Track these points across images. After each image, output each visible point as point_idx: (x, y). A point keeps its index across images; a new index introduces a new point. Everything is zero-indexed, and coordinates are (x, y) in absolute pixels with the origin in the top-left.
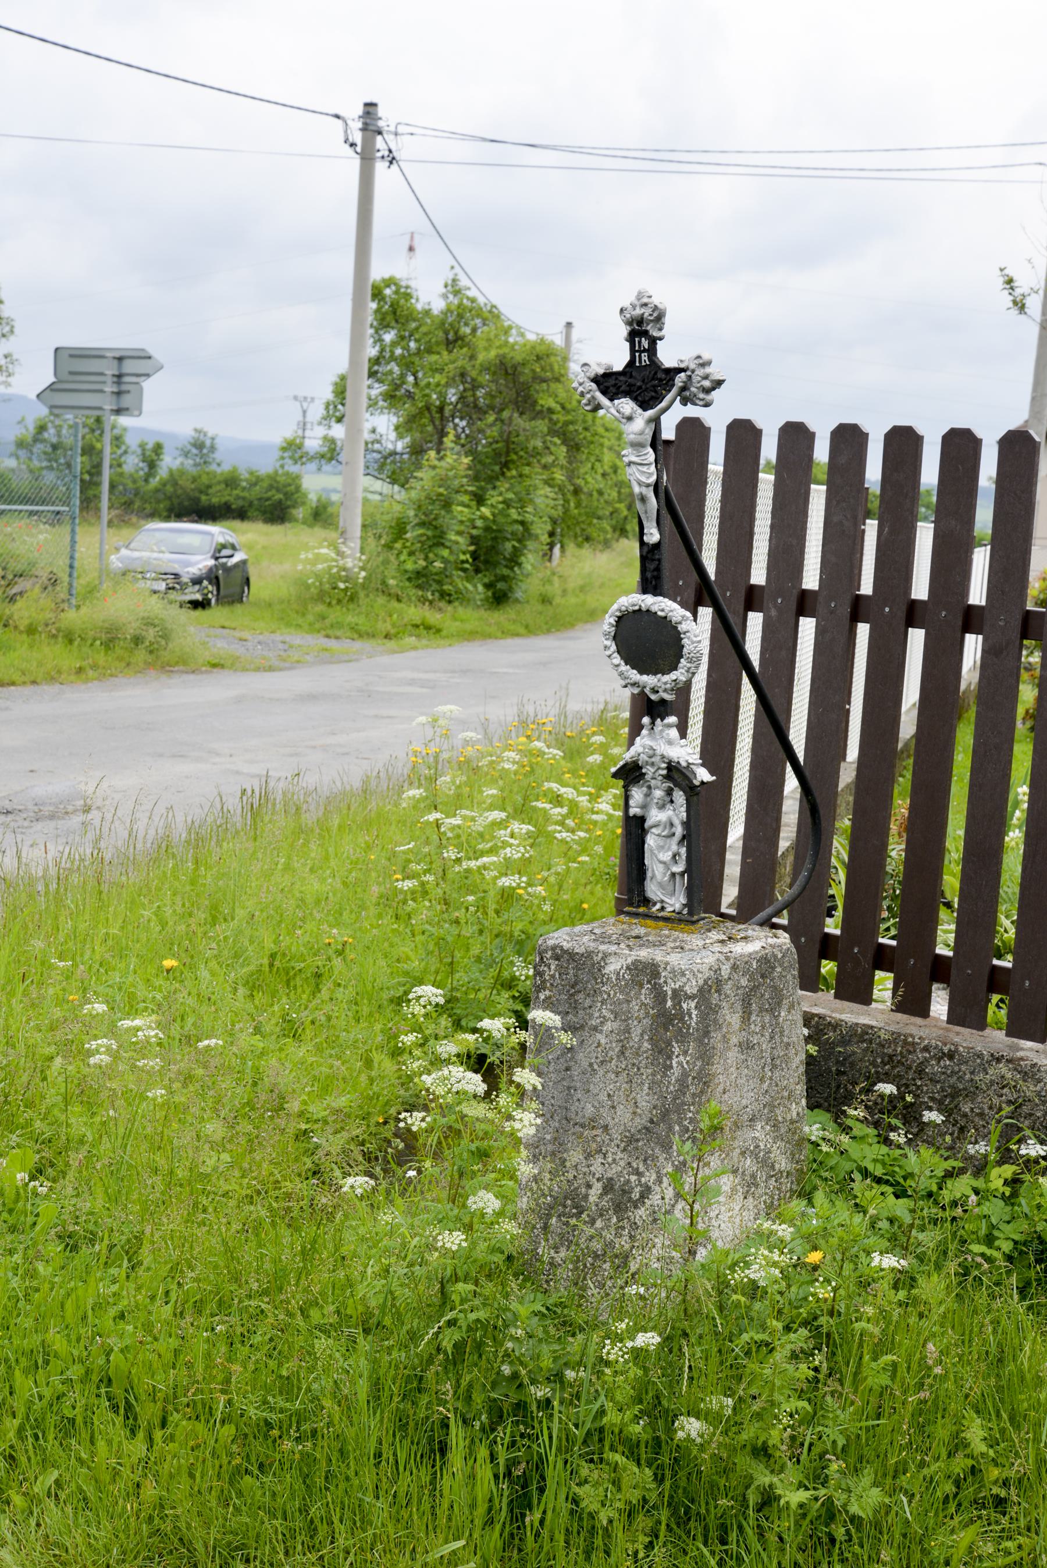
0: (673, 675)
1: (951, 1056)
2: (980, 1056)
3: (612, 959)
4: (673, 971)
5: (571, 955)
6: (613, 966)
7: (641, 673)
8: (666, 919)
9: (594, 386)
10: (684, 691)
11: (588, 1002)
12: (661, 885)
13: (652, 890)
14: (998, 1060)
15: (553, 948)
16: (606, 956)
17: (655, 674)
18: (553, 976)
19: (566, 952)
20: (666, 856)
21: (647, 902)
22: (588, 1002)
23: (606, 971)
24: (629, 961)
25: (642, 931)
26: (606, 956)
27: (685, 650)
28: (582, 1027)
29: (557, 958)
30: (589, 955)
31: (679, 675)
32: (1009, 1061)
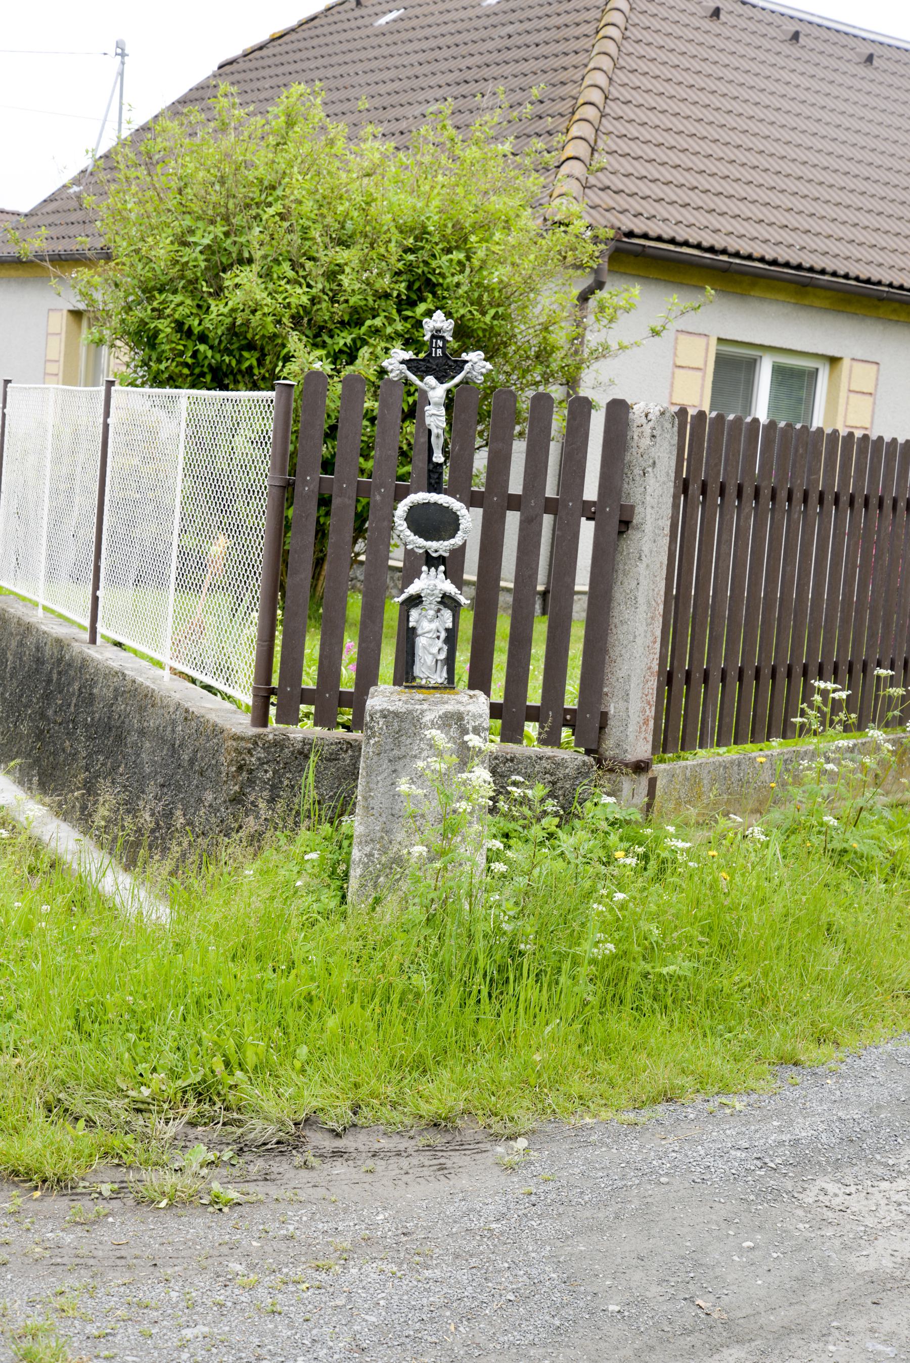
0: (452, 541)
1: (512, 760)
2: (530, 758)
3: (428, 713)
4: (474, 716)
5: (396, 714)
6: (428, 718)
7: (427, 539)
8: (434, 688)
9: (404, 367)
10: (459, 553)
11: (409, 741)
12: (429, 668)
13: (418, 670)
14: (541, 759)
15: (382, 711)
16: (422, 712)
17: (438, 540)
18: (381, 729)
19: (393, 712)
20: (435, 650)
21: (414, 678)
22: (408, 742)
23: (424, 720)
24: (441, 713)
25: (421, 697)
26: (422, 712)
27: (461, 527)
28: (404, 756)
29: (385, 717)
30: (410, 712)
31: (457, 541)
32: (548, 758)
